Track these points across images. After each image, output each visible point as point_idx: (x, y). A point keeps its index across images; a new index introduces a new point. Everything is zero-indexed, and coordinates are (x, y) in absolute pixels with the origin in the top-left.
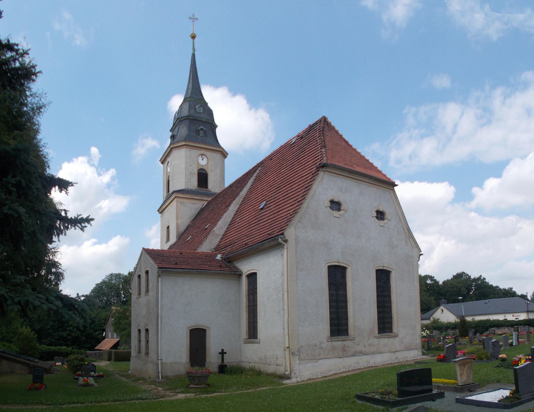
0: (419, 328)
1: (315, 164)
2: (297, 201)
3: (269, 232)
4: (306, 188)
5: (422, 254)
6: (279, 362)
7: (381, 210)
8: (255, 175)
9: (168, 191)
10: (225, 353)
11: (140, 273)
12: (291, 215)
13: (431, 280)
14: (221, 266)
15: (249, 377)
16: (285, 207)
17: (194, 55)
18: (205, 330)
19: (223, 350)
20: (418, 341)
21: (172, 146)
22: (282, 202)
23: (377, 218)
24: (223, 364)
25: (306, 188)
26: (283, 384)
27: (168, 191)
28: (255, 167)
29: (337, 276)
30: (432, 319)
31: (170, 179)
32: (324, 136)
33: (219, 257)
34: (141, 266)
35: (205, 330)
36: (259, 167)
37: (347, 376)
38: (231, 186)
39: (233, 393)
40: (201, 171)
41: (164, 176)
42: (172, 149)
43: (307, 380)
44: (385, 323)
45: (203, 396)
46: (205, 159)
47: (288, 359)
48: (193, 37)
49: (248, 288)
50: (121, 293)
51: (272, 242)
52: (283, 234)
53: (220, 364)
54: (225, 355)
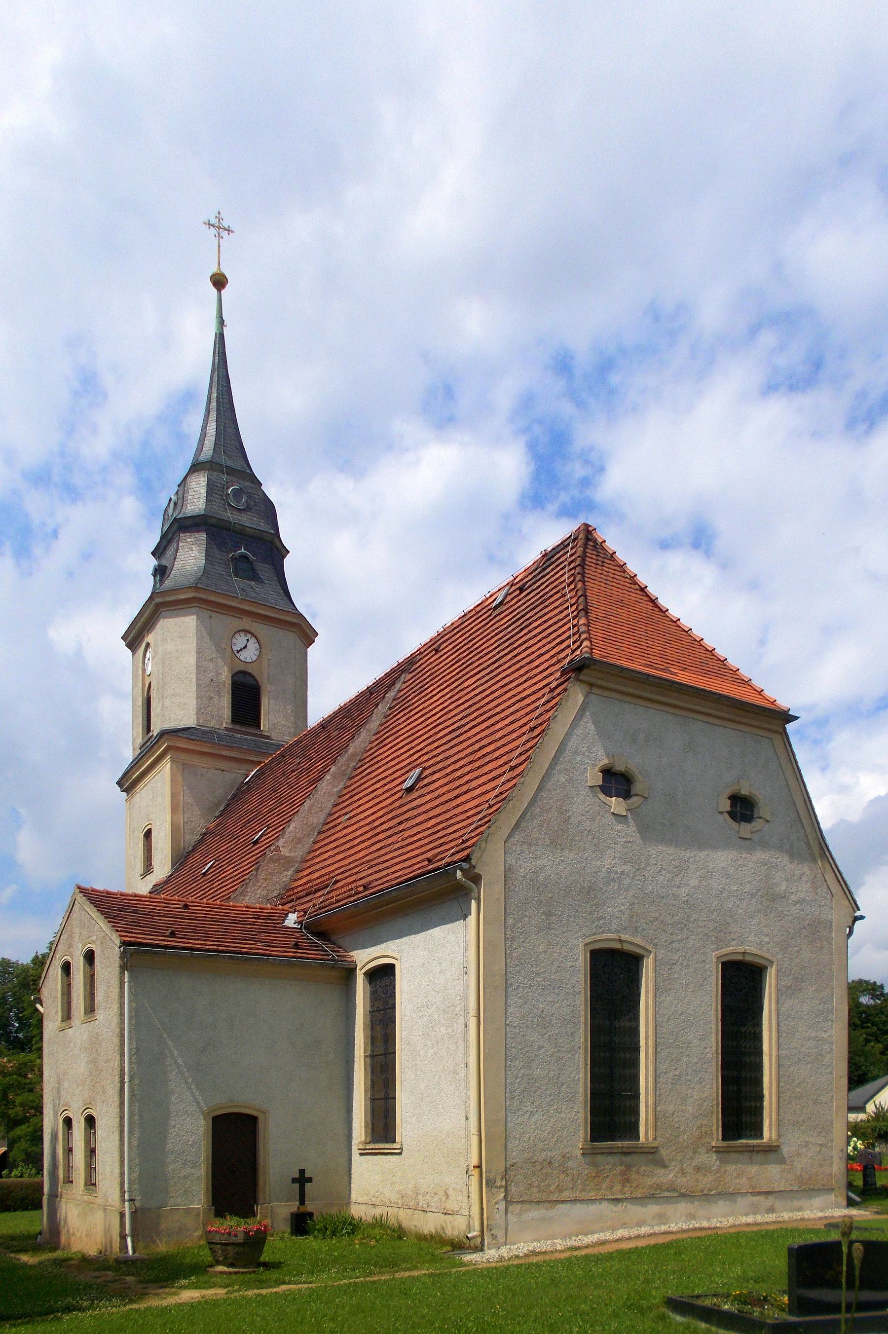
0: (839, 1131)
1: (559, 661)
2: (507, 767)
3: (429, 855)
4: (532, 729)
5: (862, 918)
6: (451, 1205)
7: (744, 792)
8: (391, 695)
9: (148, 728)
10: (310, 1180)
11: (69, 958)
12: (490, 807)
13: (874, 997)
14: (296, 946)
15: (373, 1243)
16: (474, 784)
17: (220, 338)
18: (254, 1119)
19: (302, 1172)
20: (838, 1167)
21: (158, 600)
22: (467, 769)
23: (732, 815)
24: (302, 1209)
25: (532, 729)
26: (462, 1264)
27: (148, 728)
28: (393, 671)
29: (614, 977)
30: (870, 1108)
31: (153, 694)
32: (584, 582)
33: (292, 920)
34: (71, 937)
35: (254, 1119)
36: (403, 671)
37: (637, 1248)
38: (324, 725)
39: (330, 1283)
40: (241, 678)
41: (134, 686)
42: (158, 606)
43: (526, 1255)
44: (740, 1111)
45: (250, 1293)
46: (253, 646)
47: (475, 1196)
48: (219, 282)
49: (372, 1006)
50: (8, 1018)
51: (437, 892)
52: (467, 859)
53: (294, 1209)
54: (308, 1185)
